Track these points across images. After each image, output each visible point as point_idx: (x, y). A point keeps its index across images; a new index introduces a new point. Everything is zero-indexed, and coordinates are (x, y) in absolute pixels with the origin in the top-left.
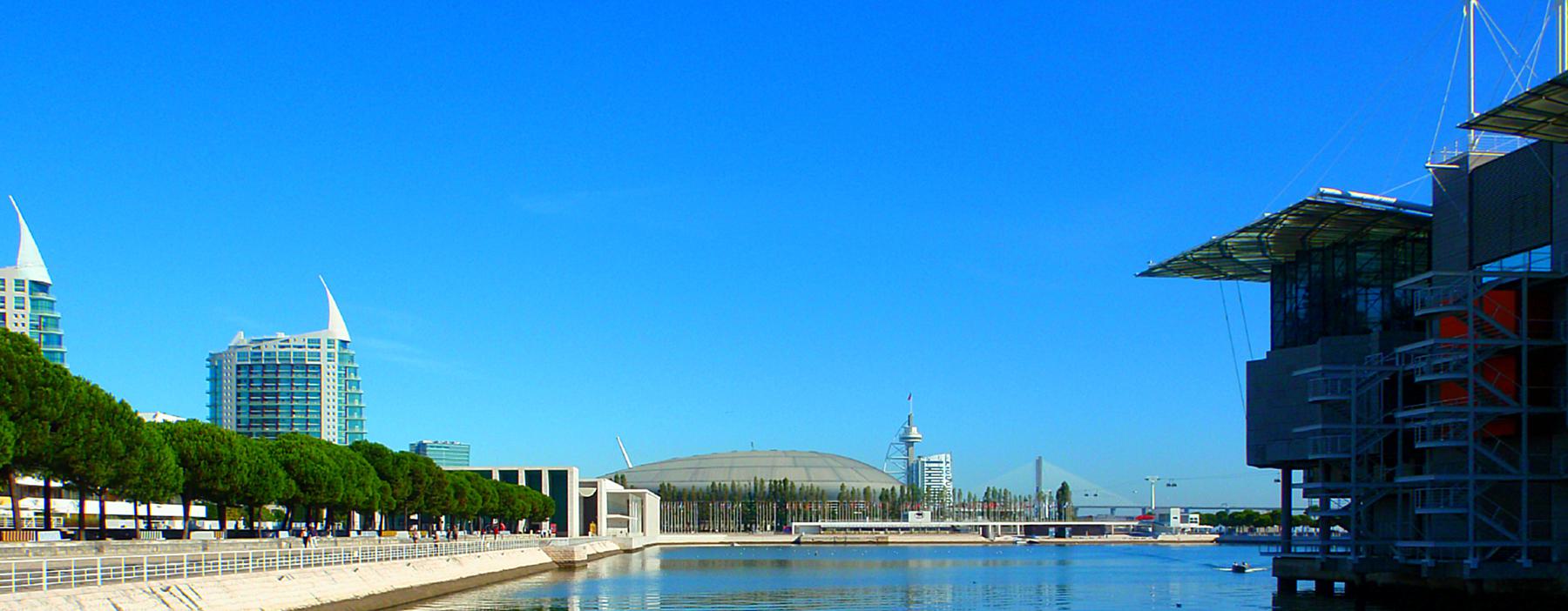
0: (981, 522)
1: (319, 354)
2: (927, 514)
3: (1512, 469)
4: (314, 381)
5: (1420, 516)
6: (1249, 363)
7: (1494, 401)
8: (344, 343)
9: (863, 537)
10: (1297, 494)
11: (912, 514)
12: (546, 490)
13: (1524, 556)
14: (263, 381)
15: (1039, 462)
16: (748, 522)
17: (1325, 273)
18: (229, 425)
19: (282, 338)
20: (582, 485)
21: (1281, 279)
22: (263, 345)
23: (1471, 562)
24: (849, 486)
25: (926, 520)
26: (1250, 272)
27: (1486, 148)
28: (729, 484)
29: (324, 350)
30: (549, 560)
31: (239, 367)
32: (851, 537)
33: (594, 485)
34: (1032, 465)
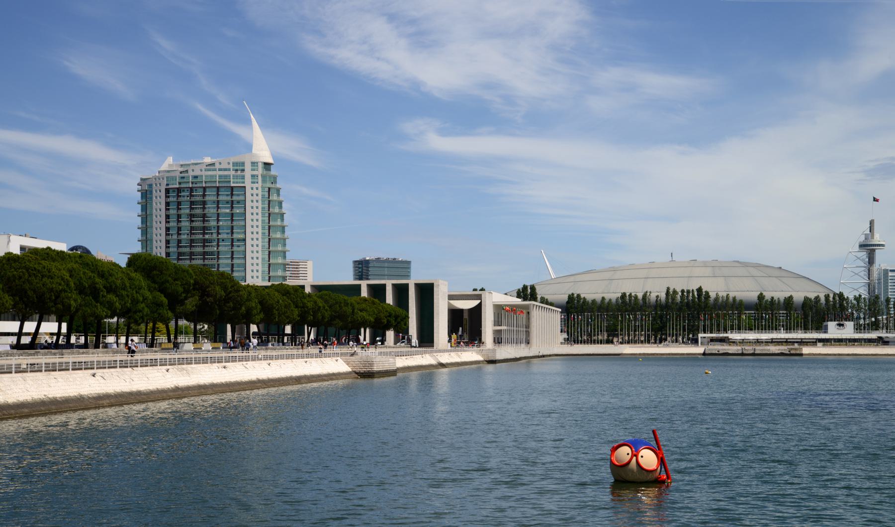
1: (243, 177)
2: (850, 325)
6: (409, 263)
8: (267, 165)
12: (390, 299)
14: (194, 205)
16: (659, 334)
18: (159, 250)
19: (207, 162)
24: (768, 296)
27: (166, 44)
28: (640, 296)
29: (248, 173)
31: (167, 191)
32: (759, 349)
33: (479, 297)
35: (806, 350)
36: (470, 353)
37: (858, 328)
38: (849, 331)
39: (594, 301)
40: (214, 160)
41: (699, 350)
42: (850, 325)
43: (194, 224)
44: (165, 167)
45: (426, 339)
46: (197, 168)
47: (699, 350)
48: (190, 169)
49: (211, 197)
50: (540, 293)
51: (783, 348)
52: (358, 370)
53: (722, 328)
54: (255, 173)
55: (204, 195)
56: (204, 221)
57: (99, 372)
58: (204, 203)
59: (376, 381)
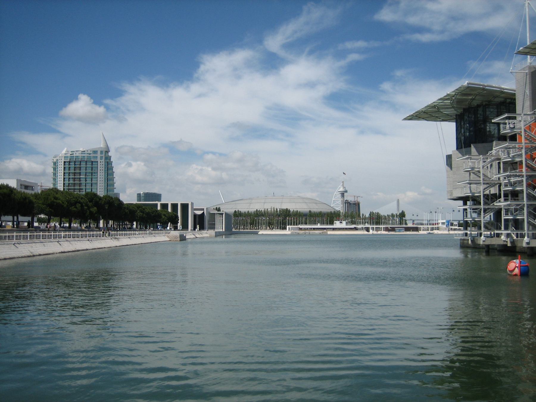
0: (367, 225)
1: (97, 157)
2: (344, 222)
4: (95, 168)
6: (161, 195)
9: (317, 232)
12: (170, 210)
18: (60, 187)
21: (459, 120)
22: (74, 153)
25: (344, 225)
26: (446, 118)
29: (99, 155)
31: (65, 162)
34: (396, 202)
35: (329, 232)
38: (344, 225)
39: (245, 212)
42: (344, 222)
43: (75, 182)
45: (185, 226)
46: (77, 153)
48: (74, 153)
49: (83, 165)
54: (102, 155)
55: (80, 164)
56: (80, 186)
58: (80, 168)
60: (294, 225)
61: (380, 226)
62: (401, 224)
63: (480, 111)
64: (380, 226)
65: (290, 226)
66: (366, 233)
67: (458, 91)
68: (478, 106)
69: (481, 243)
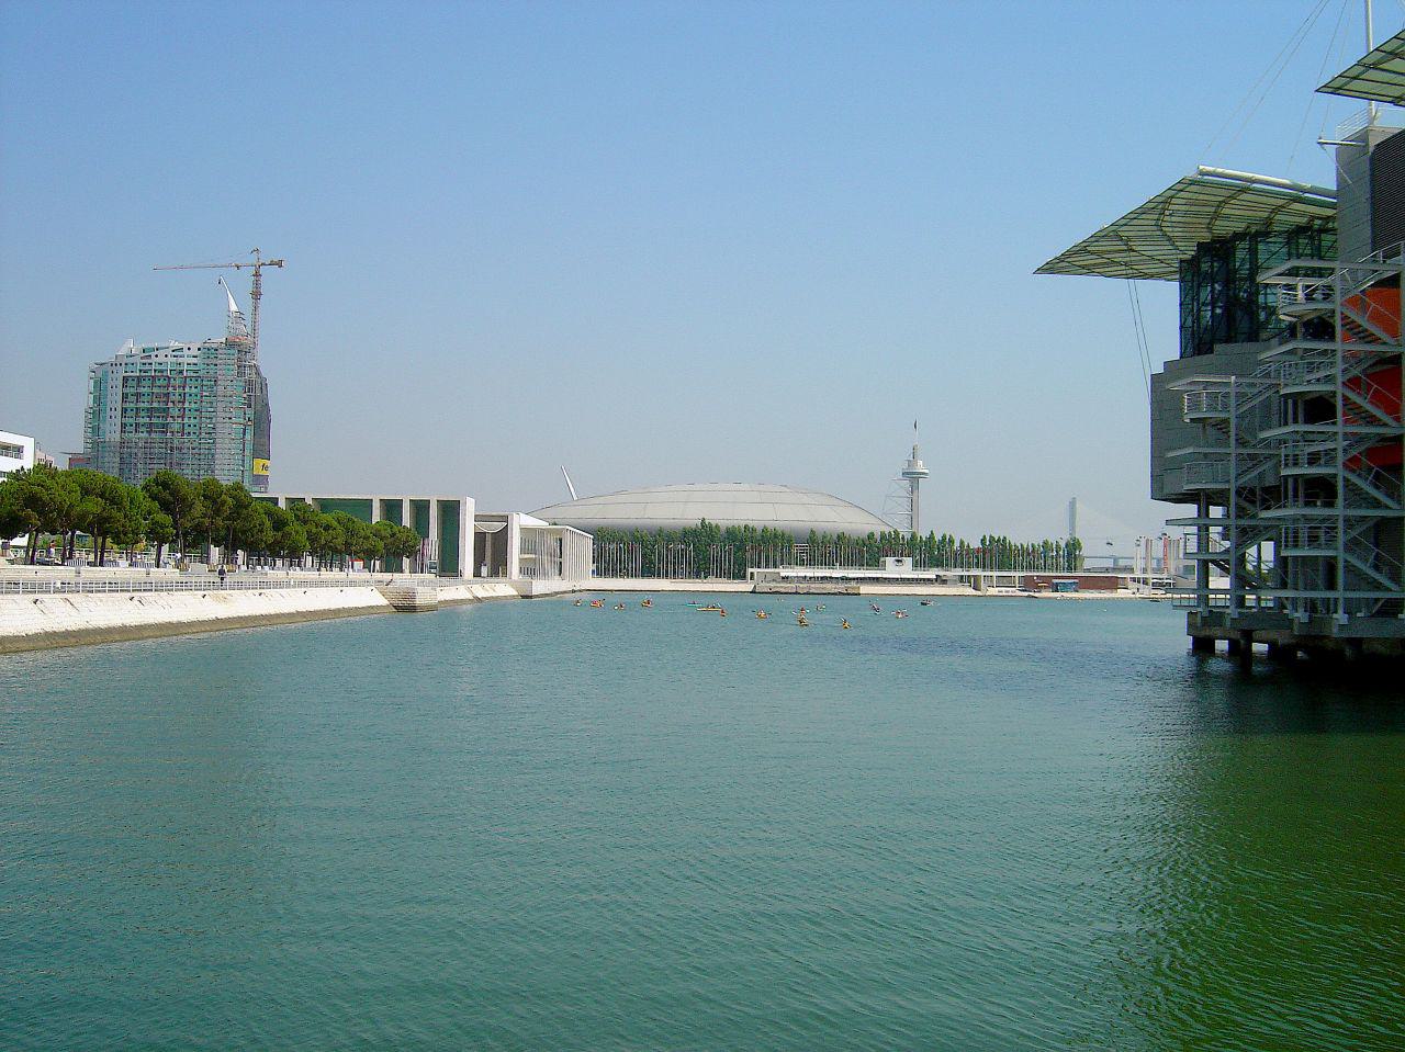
2: (908, 561)
3: (1389, 502)
5: (1286, 558)
7: (1372, 420)
9: (830, 587)
10: (1215, 531)
11: (890, 560)
12: (407, 521)
13: (1340, 611)
15: (1072, 504)
16: (700, 570)
17: (1223, 267)
20: (477, 518)
21: (1191, 274)
23: (1340, 617)
30: (384, 602)
31: (125, 379)
33: (505, 519)
35: (864, 589)
36: (502, 585)
37: (916, 565)
40: (181, 345)
41: (747, 586)
42: (908, 561)
44: (123, 351)
45: (448, 566)
47: (747, 586)
50: (1094, 557)
51: (841, 587)
52: (396, 603)
53: (771, 563)
57: (309, 590)
59: (419, 615)
60: (767, 566)
61: (1012, 574)
62: (1070, 569)
63: (1241, 253)
64: (1012, 574)
65: (755, 570)
66: (970, 591)
67: (1189, 278)
68: (1238, 236)
69: (1335, 632)
